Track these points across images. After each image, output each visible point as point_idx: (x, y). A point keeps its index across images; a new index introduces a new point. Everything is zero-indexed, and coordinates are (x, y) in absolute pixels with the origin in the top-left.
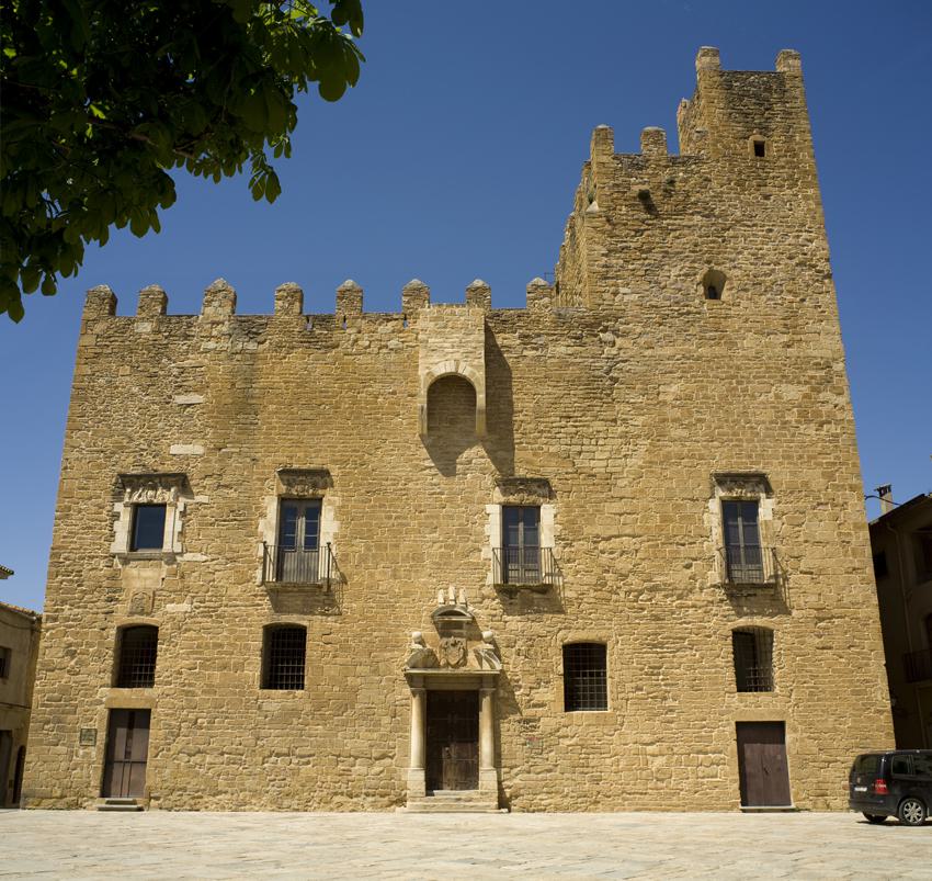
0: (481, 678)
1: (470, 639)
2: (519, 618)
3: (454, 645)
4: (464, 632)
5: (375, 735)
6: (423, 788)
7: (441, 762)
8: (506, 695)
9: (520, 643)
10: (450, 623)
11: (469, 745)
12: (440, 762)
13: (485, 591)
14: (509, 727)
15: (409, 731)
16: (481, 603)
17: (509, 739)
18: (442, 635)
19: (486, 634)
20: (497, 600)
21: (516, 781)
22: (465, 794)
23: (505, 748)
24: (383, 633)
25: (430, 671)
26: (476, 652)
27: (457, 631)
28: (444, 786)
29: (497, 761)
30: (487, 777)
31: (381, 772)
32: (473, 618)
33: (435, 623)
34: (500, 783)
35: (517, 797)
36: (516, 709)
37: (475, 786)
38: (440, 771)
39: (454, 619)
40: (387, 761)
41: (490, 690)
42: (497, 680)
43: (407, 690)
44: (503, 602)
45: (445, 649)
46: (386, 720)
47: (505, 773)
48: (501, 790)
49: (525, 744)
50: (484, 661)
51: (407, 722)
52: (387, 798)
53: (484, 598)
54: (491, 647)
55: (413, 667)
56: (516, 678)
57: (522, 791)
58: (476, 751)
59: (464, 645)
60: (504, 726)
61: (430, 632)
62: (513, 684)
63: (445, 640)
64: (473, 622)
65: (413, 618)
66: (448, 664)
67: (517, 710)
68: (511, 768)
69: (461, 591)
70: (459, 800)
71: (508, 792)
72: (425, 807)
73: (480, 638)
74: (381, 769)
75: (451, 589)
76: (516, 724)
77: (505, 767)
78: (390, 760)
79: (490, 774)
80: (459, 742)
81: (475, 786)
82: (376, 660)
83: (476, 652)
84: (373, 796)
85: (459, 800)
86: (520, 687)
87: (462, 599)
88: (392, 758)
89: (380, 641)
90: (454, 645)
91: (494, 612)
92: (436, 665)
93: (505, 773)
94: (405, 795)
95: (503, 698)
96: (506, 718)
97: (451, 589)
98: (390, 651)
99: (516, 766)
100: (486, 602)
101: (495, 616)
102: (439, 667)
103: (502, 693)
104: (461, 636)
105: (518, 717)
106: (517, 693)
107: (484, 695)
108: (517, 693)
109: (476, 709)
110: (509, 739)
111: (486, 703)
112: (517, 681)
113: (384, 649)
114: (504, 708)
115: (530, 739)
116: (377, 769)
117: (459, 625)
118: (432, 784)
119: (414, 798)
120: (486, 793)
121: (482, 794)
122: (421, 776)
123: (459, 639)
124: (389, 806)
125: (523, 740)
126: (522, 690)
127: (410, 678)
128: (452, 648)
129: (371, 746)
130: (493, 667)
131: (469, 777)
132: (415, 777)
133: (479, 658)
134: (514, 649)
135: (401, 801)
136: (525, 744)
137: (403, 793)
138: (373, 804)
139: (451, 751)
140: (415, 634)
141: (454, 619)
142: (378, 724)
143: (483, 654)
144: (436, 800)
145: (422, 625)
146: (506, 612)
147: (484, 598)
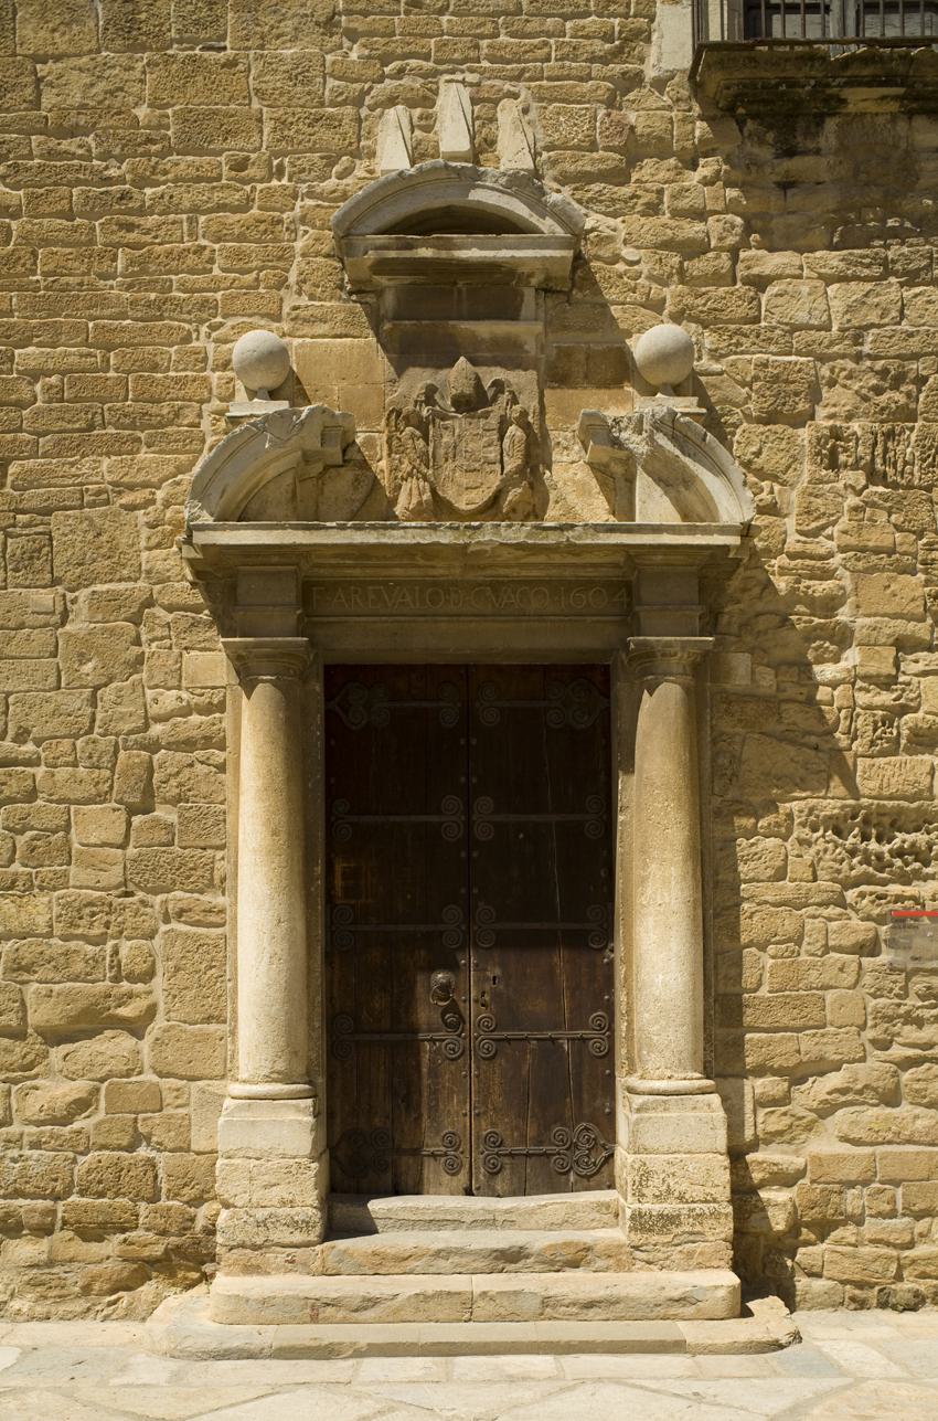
0: (628, 582)
1: (557, 376)
2: (833, 260)
3: (473, 403)
4: (526, 331)
5: (40, 909)
6: (304, 1195)
7: (413, 1048)
8: (767, 681)
9: (838, 399)
10: (439, 280)
11: (560, 959)
12: (403, 1043)
13: (641, 114)
14: (782, 855)
15: (225, 884)
16: (619, 176)
17: (787, 923)
18: (406, 352)
19: (649, 340)
20: (707, 167)
21: (824, 1144)
22: (542, 1217)
23: (761, 970)
24: (70, 353)
25: (333, 536)
26: (598, 432)
27: (484, 329)
28: (431, 1170)
29: (722, 1044)
30: (667, 1127)
31: (82, 1105)
32: (579, 260)
33: (359, 290)
34: (737, 1155)
35: (823, 1229)
36: (824, 759)
37: (595, 1169)
38: (406, 1093)
39: (473, 251)
40: (111, 1047)
41: (677, 643)
42: (714, 583)
43: (211, 663)
44: (743, 173)
45: (423, 426)
46: (97, 825)
47: (759, 1103)
48: (744, 1194)
49: (869, 948)
50: (643, 482)
51: (214, 830)
52: (112, 1245)
53: (635, 149)
54: (685, 405)
55: (242, 514)
56: (821, 588)
57: (853, 1200)
58: (598, 990)
59: (529, 402)
60: (758, 852)
61: (344, 357)
62: (802, 619)
63: (418, 379)
64: (574, 283)
65: (238, 262)
66: (438, 508)
67: (834, 765)
68: (796, 1076)
69: (507, 113)
70: (510, 1258)
71: (778, 1203)
72: (316, 1310)
73: (619, 370)
74: (79, 1088)
75: (452, 104)
76: (823, 840)
77: (760, 1071)
78: (126, 1042)
79: (676, 1112)
80: (505, 942)
81: (595, 1169)
82: (34, 497)
83: (598, 432)
84: (44, 1230)
85: (510, 1258)
86: (843, 638)
87: (512, 153)
88: (136, 1028)
89: (56, 395)
90: (473, 403)
91: (693, 229)
92: (372, 504)
93: (759, 1103)
94: (211, 1231)
95: (21, 1294)
96: (771, 806)
97: (452, 104)
98: (113, 448)
99: (822, 1067)
100: (650, 172)
101: (696, 249)
102: (387, 516)
103: (740, 668)
104: (509, 354)
105: (831, 803)
106: (825, 672)
107: (648, 670)
108: (825, 672)
109: (596, 761)
110: (787, 923)
111: (657, 727)
112: (830, 605)
113: (82, 440)
114: (756, 754)
115: (899, 920)
116: (55, 1091)
117: (495, 291)
118: (361, 1166)
119: (254, 1256)
120: (671, 1220)
121: (640, 1222)
122: (291, 1130)
123: (490, 375)
124: (128, 1286)
125: (859, 928)
126: (852, 657)
127: (225, 583)
128: (459, 422)
129: (19, 968)
130: (695, 511)
131: (559, 1122)
132: (259, 1134)
133: (616, 480)
134: (805, 434)
135: (188, 1260)
136: (869, 948)
137: (203, 1213)
138: (44, 1281)
139: (464, 995)
140: (253, 340)
141: (473, 251)
142: (54, 847)
143: (637, 444)
144: (380, 1264)
145: (291, 300)
146: (762, 229)
147: (635, 149)
